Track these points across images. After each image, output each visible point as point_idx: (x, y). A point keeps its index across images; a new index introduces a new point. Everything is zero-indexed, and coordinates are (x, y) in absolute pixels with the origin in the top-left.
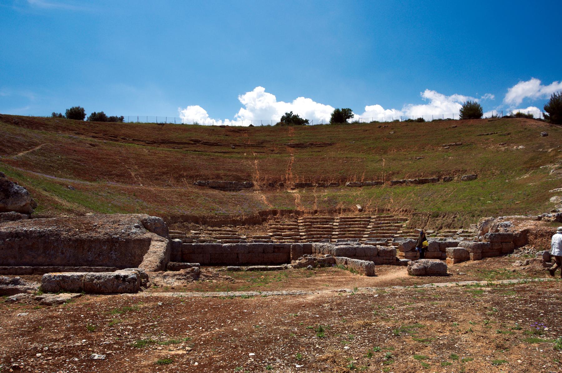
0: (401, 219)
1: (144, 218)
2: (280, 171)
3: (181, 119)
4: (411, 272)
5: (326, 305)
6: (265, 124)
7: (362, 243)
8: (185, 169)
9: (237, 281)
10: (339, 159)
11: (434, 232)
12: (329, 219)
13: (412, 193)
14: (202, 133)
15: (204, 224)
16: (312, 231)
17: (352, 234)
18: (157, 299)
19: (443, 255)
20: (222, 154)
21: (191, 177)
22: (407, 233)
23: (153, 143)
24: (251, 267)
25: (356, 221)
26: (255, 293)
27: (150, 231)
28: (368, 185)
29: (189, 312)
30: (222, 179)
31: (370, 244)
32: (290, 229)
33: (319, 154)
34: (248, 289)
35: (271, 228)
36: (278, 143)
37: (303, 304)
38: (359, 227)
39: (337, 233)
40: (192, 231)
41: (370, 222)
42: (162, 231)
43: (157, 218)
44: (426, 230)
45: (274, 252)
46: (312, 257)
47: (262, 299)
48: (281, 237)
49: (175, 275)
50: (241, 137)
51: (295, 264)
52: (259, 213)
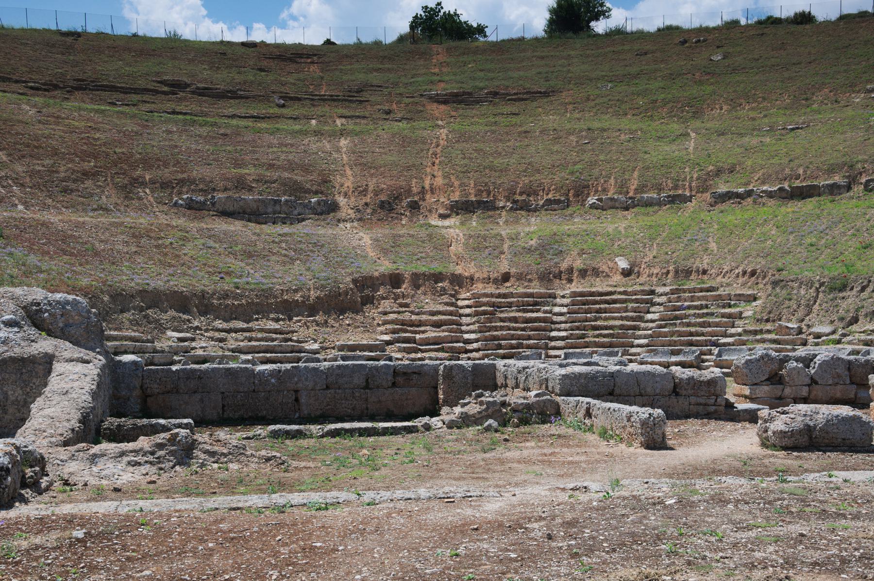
0: (739, 297)
1: (30, 299)
2: (408, 168)
3: (128, 22)
4: (767, 439)
5: (536, 525)
6: (367, 39)
7: (631, 361)
8: (147, 163)
9: (295, 464)
10: (569, 133)
11: (834, 332)
12: (541, 296)
13: (769, 227)
14: (191, 61)
15: (203, 313)
16: (496, 329)
17: (605, 336)
18: (70, 521)
19: (862, 394)
20: (249, 123)
21: (165, 185)
22: (755, 333)
23: (49, 87)
24: (333, 426)
25: (615, 302)
26: (343, 496)
27: (50, 334)
28: (649, 204)
29: (162, 552)
30: (250, 189)
31: (651, 363)
32: (437, 325)
33: (514, 120)
34: (327, 484)
35: (385, 323)
36: (402, 90)
37: (473, 523)
38: (622, 318)
39: (564, 334)
40: (170, 333)
41: (654, 304)
42: (85, 332)
43: (71, 297)
44: (809, 326)
45: (394, 384)
46: (497, 396)
47: (365, 512)
48: (413, 346)
49: (123, 454)
50: (301, 76)
51: (452, 417)
52: (355, 281)
